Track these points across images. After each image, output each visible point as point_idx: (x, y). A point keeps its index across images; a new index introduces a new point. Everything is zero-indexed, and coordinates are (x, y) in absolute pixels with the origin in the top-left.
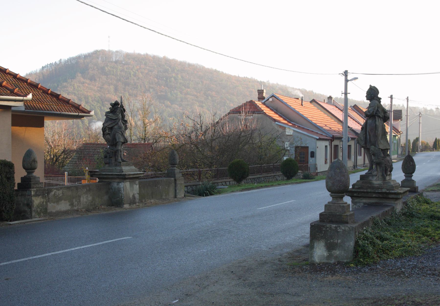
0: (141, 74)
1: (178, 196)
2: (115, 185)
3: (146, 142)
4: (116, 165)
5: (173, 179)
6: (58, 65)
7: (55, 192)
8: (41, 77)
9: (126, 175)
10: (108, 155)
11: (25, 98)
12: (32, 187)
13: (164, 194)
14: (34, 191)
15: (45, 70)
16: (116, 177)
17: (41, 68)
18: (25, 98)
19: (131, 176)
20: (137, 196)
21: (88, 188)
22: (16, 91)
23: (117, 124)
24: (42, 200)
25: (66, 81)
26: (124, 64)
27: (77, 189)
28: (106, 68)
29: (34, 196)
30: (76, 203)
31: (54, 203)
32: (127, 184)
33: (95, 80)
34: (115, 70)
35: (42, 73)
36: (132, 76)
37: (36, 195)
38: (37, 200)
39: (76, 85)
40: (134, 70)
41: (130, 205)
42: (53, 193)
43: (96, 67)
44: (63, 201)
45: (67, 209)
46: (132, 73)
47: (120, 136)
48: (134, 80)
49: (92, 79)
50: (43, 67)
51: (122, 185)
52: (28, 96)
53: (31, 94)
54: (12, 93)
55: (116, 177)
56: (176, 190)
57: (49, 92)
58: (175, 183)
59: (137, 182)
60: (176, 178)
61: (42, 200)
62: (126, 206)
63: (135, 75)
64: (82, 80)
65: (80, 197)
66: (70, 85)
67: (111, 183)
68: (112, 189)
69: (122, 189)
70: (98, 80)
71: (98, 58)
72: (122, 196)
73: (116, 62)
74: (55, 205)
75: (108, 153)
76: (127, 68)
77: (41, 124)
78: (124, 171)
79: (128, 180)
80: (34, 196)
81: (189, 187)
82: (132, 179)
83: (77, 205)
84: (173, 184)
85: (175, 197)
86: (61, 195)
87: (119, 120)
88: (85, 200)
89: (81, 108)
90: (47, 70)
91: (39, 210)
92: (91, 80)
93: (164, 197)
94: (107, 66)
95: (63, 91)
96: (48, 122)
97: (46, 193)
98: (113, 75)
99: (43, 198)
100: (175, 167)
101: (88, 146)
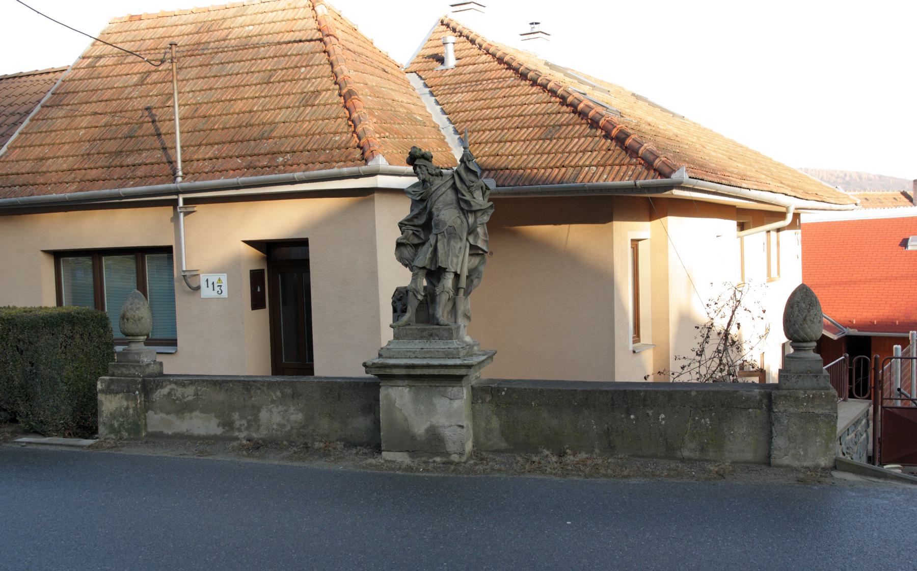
7: (172, 390)
14: (103, 381)
19: (418, 372)
21: (289, 391)
24: (125, 403)
27: (248, 390)
29: (102, 391)
30: (244, 422)
31: (168, 413)
37: (108, 391)
38: (111, 402)
42: (165, 391)
44: (197, 413)
45: (212, 433)
56: (770, 437)
57: (614, 132)
65: (257, 409)
74: (172, 417)
79: (406, 382)
80: (102, 391)
83: (248, 428)
86: (191, 398)
88: (277, 419)
89: (657, 163)
91: (116, 425)
99: (127, 399)
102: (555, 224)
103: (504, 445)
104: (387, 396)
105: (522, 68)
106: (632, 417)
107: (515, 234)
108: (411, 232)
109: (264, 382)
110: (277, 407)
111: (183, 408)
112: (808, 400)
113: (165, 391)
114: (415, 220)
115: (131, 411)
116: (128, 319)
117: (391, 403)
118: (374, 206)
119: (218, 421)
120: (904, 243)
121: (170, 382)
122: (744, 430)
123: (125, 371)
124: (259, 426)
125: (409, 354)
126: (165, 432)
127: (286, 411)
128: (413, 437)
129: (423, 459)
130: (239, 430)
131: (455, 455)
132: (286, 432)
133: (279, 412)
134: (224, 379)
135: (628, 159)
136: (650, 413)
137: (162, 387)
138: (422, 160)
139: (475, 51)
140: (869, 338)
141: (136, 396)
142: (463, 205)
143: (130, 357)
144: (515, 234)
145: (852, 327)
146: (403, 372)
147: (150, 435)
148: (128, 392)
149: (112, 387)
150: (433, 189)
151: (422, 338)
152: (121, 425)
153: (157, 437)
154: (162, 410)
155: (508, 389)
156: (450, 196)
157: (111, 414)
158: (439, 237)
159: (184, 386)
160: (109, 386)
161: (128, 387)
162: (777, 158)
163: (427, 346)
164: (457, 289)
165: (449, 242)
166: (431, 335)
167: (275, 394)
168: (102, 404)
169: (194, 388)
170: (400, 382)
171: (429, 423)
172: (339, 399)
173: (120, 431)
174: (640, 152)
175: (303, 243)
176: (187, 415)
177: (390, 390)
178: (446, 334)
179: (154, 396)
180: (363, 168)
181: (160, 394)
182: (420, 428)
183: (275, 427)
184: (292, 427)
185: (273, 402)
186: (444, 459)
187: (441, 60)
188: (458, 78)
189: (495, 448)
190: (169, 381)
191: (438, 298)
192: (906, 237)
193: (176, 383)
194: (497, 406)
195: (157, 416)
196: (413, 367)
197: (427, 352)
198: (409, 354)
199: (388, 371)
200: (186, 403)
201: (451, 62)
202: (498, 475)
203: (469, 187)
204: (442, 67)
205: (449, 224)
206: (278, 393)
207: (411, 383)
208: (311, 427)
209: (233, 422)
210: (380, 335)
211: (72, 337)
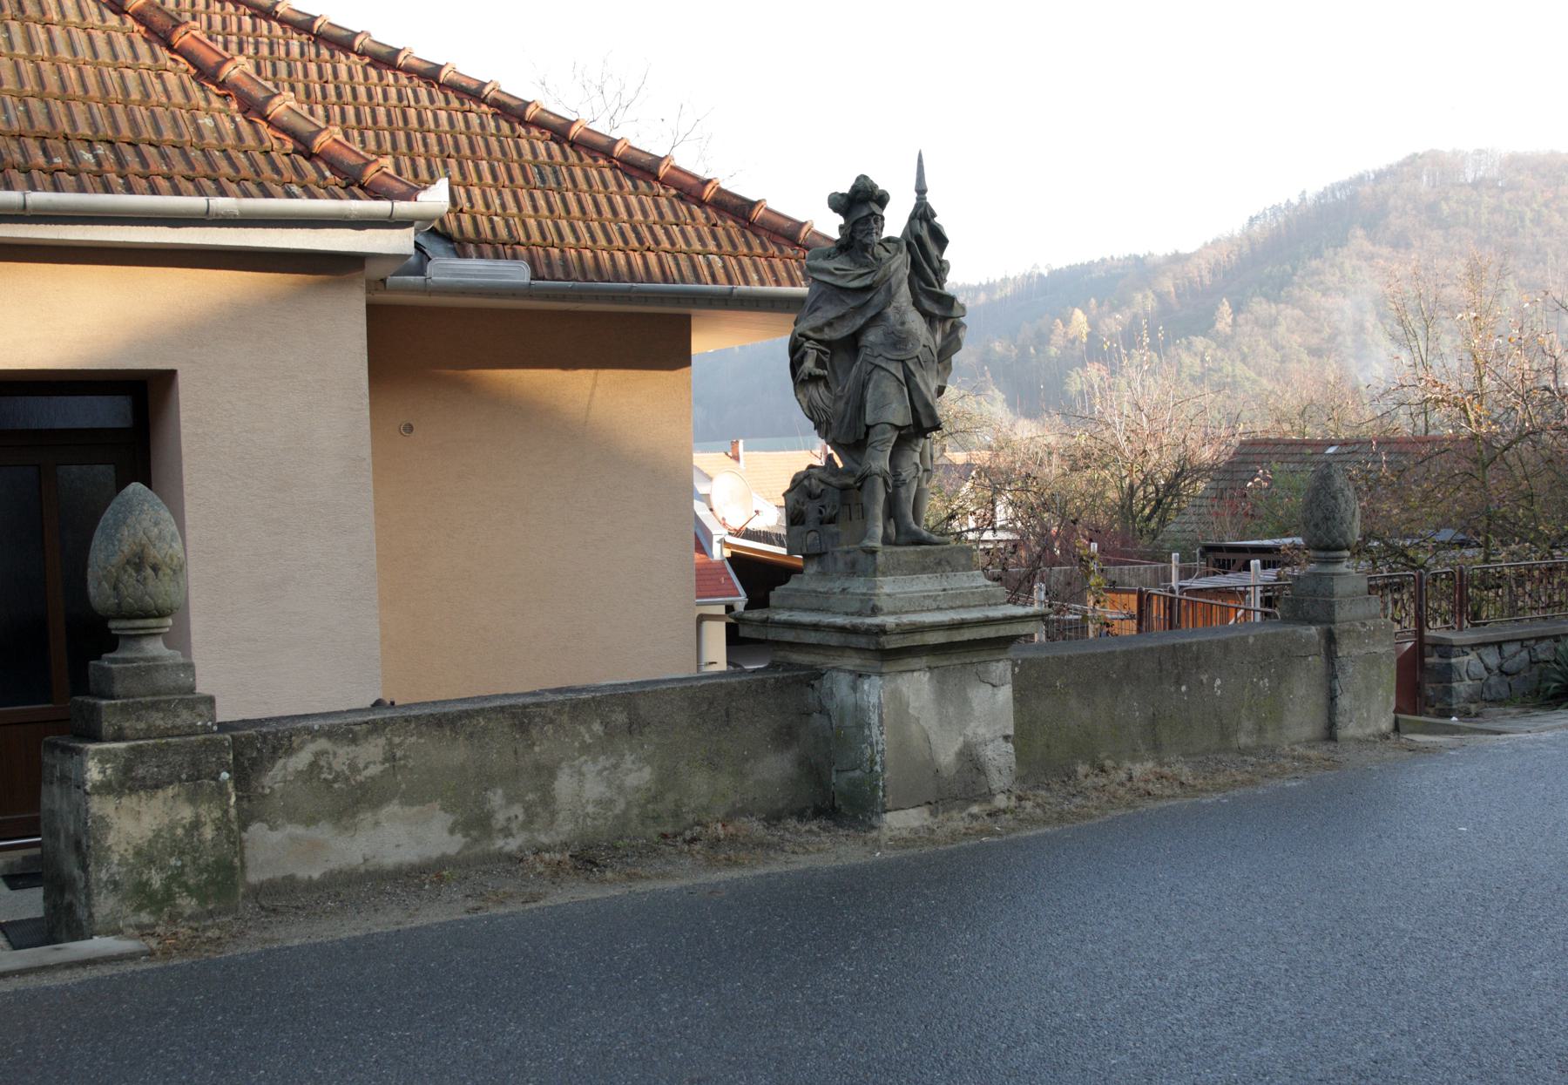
0: (1557, 216)
1: (1349, 729)
2: (840, 688)
3: (1484, 430)
4: (853, 570)
5: (1313, 630)
6: (1296, 209)
7: (318, 754)
8: (1246, 249)
9: (882, 630)
10: (811, 508)
11: (403, 207)
12: (107, 728)
13: (1248, 725)
14: (104, 758)
15: (1256, 228)
16: (835, 639)
17: (1246, 221)
18: (403, 207)
20: (999, 756)
21: (620, 718)
22: (370, 174)
23: (878, 317)
24: (186, 813)
25: (1317, 254)
26: (1503, 190)
28: (1444, 206)
29: (105, 788)
30: (517, 810)
31: (311, 821)
32: (915, 688)
33: (1408, 246)
34: (1471, 211)
35: (1249, 238)
36: (1528, 222)
37: (126, 783)
39: (1347, 265)
40: (1535, 206)
41: (933, 814)
43: (1410, 206)
44: (393, 808)
45: (435, 853)
46: (1529, 215)
47: (890, 388)
48: (1534, 236)
49: (1400, 242)
50: (1252, 220)
51: (874, 691)
52: (422, 196)
53: (442, 185)
54: (353, 181)
55: (835, 639)
56: (1332, 698)
57: (708, 193)
58: (1331, 656)
59: (1001, 668)
60: (1337, 628)
61: (186, 813)
62: (901, 821)
63: (1537, 221)
64: (1368, 247)
65: (546, 772)
66: (1332, 266)
67: (819, 675)
68: (824, 711)
69: (875, 719)
70: (1417, 243)
71: (1418, 177)
72: (873, 762)
73: (1476, 185)
74: (323, 831)
75: (811, 496)
76: (1510, 201)
77: (675, 354)
78: (882, 602)
79: (924, 661)
80: (105, 788)
81: (1509, 649)
82: (958, 650)
84: (1317, 662)
85: (1330, 733)
86: (374, 770)
87: (890, 295)
88: (594, 788)
90: (1262, 227)
91: (157, 880)
92: (1395, 246)
93: (1243, 740)
94: (1446, 199)
95: (1310, 286)
96: (706, 342)
97: (224, 766)
98: (1466, 225)
99: (192, 799)
100: (1338, 561)
101: (1259, 449)
102: (565, 366)
105: (318, 23)
106: (1184, 688)
107: (466, 387)
109: (563, 703)
110: (595, 761)
111: (351, 801)
112: (1371, 634)
113: (301, 760)
114: (826, 330)
115: (208, 833)
116: (155, 569)
119: (449, 819)
121: (314, 734)
122: (1302, 692)
123: (159, 720)
124: (553, 814)
125: (927, 602)
126: (302, 873)
127: (616, 766)
130: (507, 832)
132: (617, 817)
133: (600, 773)
134: (466, 707)
136: (1204, 678)
137: (290, 751)
141: (221, 787)
143: (163, 680)
144: (466, 387)
147: (256, 892)
148: (195, 778)
149: (140, 771)
152: (176, 877)
153: (283, 896)
154: (292, 815)
157: (138, 853)
159: (354, 741)
160: (127, 769)
161: (193, 764)
162: (1060, 263)
166: (939, 563)
167: (589, 730)
168: (108, 827)
169: (382, 741)
172: (728, 723)
173: (169, 896)
175: (167, 378)
176: (367, 817)
177: (899, 680)
179: (266, 781)
181: (280, 774)
183: (590, 809)
184: (628, 803)
185: (585, 749)
186: (988, 807)
190: (309, 731)
193: (330, 734)
195: (276, 836)
196: (962, 625)
197: (956, 596)
198: (927, 602)
200: (361, 785)
202: (1172, 803)
206: (597, 727)
208: (671, 797)
209: (490, 815)
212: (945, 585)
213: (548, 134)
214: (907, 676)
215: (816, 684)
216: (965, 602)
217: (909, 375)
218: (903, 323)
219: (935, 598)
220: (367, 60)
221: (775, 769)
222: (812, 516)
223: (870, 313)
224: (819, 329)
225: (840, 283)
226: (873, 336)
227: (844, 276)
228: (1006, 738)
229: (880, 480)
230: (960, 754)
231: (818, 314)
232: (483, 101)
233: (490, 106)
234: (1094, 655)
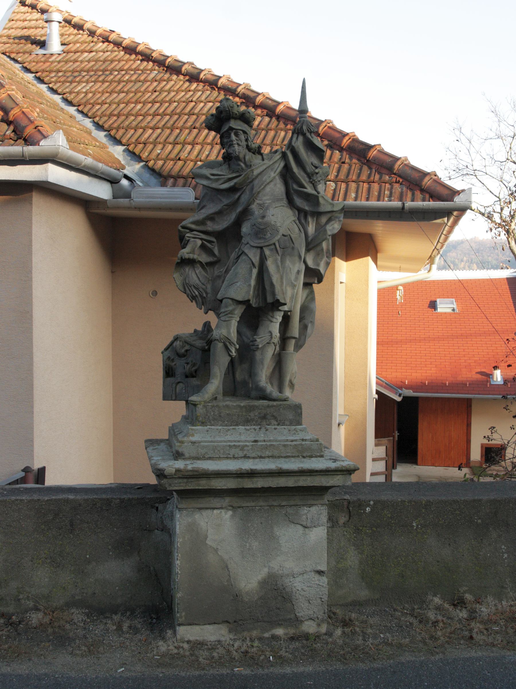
10: (180, 366)
19: (260, 483)
23: (246, 213)
57: (345, 142)
79: (227, 501)
103: (364, 594)
104: (192, 528)
108: (199, 242)
114: (209, 223)
117: (198, 540)
118: (31, 211)
120: (433, 305)
128: (237, 597)
129: (255, 633)
131: (310, 623)
135: (377, 177)
138: (239, 123)
139: (84, 37)
140: (416, 399)
142: (299, 202)
145: (408, 387)
146: (231, 484)
150: (256, 173)
151: (247, 422)
155: (376, 502)
156: (278, 187)
158: (267, 252)
163: (261, 436)
164: (284, 339)
165: (283, 261)
166: (264, 417)
170: (216, 502)
171: (266, 570)
174: (396, 167)
177: (197, 516)
178: (290, 415)
180: (31, 150)
182: (249, 580)
186: (292, 631)
187: (42, 44)
188: (70, 66)
189: (350, 600)
191: (258, 354)
192: (433, 299)
194: (358, 531)
196: (252, 474)
197: (266, 447)
198: (233, 451)
199: (203, 484)
201: (55, 46)
203: (310, 176)
204: (41, 52)
205: (282, 231)
207: (236, 501)
210: (32, 407)
211: (308, 647)
212: (261, 436)
213: (265, 112)
214: (205, 513)
215: (160, 507)
216: (276, 453)
217: (263, 259)
218: (263, 217)
219: (242, 448)
220: (187, 78)
221: (114, 572)
222: (179, 371)
223: (239, 209)
224: (201, 222)
225: (215, 185)
226: (245, 229)
227: (217, 180)
228: (320, 573)
229: (220, 345)
230: (264, 583)
231: (203, 211)
232: (237, 96)
233: (240, 98)
234: (455, 502)
